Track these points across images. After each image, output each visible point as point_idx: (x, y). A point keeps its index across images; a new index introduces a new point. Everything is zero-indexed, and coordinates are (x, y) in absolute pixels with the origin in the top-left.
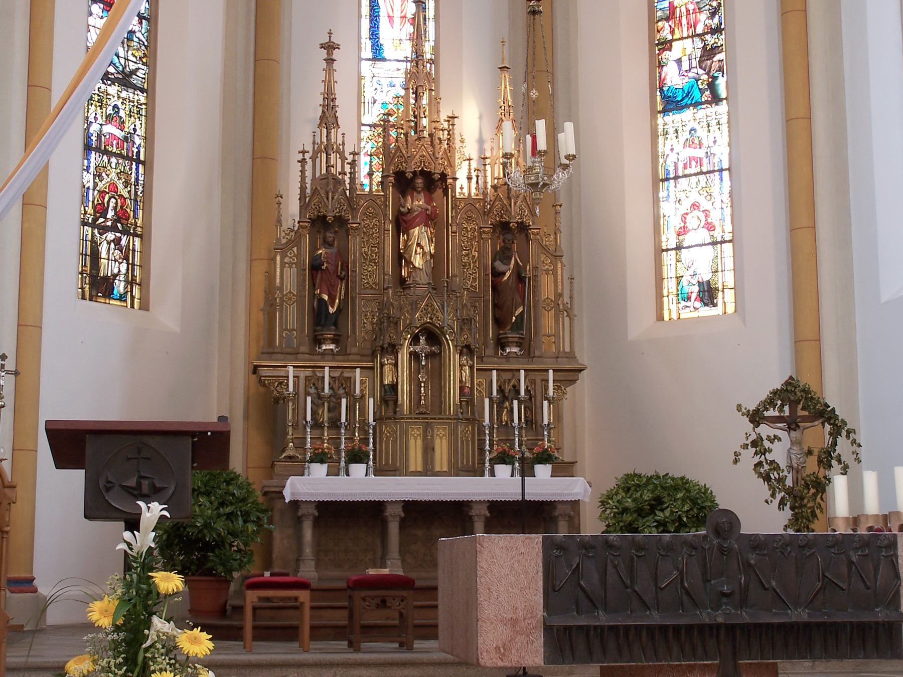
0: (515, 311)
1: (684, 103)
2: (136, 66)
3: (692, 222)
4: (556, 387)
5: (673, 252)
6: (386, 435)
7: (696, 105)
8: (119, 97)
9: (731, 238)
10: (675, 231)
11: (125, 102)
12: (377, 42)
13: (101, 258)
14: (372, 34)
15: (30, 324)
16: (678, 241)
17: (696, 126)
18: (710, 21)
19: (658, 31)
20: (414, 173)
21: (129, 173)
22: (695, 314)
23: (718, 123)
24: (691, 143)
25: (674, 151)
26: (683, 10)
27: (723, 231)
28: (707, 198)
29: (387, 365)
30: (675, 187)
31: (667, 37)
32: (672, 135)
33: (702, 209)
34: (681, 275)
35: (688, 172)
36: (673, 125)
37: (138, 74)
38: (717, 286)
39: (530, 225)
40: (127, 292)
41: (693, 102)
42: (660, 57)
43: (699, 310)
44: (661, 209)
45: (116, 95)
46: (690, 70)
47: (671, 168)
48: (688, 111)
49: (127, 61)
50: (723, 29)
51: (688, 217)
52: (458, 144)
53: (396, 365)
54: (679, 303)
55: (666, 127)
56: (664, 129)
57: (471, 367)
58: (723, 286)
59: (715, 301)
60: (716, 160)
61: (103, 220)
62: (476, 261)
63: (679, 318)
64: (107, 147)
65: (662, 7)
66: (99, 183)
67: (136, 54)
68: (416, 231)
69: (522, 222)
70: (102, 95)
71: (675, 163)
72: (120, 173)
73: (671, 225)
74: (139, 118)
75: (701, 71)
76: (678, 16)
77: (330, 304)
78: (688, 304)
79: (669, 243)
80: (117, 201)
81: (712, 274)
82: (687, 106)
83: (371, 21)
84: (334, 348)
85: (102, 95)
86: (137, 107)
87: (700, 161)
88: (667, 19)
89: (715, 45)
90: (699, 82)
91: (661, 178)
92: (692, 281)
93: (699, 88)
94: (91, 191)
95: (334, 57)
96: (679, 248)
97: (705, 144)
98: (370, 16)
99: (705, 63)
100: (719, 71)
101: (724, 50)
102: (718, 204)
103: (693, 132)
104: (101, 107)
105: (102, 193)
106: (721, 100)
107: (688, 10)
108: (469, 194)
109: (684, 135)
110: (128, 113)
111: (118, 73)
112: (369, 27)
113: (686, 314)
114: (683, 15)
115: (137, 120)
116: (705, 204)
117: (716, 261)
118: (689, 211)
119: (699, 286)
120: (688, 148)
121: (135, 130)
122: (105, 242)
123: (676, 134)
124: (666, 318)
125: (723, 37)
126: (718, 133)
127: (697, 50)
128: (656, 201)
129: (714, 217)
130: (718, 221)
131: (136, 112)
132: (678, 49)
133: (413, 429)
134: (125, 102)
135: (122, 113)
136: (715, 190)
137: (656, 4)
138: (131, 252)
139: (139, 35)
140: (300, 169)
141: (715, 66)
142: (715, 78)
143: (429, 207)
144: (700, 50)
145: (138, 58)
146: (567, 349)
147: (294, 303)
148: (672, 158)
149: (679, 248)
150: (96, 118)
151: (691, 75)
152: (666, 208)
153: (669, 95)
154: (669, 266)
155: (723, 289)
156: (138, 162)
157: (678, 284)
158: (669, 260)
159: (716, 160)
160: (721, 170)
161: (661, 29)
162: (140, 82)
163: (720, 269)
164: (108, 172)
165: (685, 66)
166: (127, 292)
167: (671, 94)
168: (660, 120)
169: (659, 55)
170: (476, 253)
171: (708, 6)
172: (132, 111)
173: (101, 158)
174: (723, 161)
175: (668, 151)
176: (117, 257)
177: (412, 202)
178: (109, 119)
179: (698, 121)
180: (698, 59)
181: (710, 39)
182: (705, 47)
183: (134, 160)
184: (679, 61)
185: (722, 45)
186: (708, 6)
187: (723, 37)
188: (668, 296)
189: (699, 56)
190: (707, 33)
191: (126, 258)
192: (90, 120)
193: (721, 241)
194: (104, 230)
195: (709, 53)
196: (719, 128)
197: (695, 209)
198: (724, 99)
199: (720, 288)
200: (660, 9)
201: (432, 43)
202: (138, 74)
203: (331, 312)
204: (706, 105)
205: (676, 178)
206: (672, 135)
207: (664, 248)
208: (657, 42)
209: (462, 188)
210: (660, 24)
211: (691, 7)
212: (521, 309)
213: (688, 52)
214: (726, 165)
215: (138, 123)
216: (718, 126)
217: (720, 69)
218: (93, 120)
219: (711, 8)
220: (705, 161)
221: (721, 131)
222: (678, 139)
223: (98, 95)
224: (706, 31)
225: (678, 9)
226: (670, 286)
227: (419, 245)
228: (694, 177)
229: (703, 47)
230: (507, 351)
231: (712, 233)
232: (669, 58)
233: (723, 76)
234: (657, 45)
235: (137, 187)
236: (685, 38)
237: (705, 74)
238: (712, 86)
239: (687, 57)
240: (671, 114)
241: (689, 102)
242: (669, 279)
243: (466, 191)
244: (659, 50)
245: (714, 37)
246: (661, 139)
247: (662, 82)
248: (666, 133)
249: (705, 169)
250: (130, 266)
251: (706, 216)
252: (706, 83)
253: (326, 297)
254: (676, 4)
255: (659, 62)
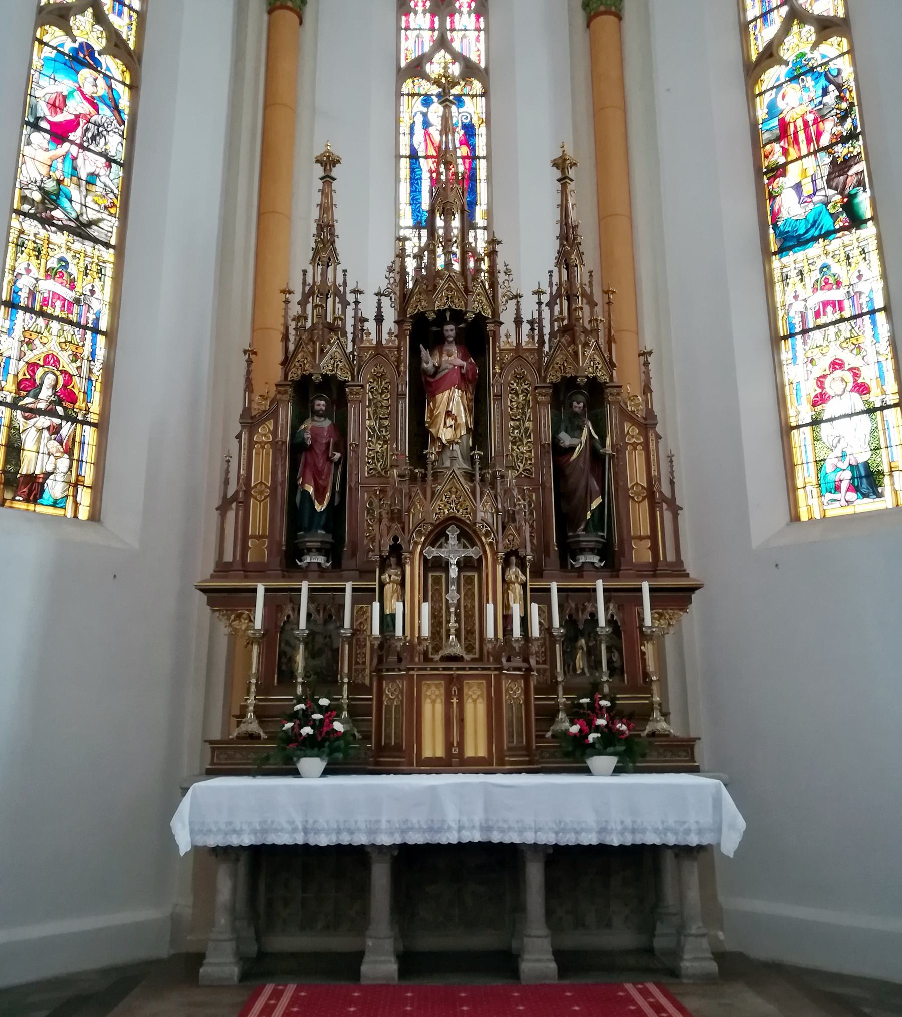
0: (591, 502)
1: (809, 236)
2: (99, 216)
3: (833, 385)
4: (657, 616)
5: (809, 429)
6: (387, 696)
7: (826, 235)
8: (69, 249)
9: (897, 401)
10: (808, 401)
11: (77, 256)
12: (419, 207)
13: (23, 450)
14: (413, 199)
15: (251, 569)
16: (814, 413)
17: (829, 261)
18: (840, 127)
19: (766, 157)
20: (441, 314)
21: (80, 344)
22: (849, 510)
23: (863, 252)
24: (824, 284)
25: (800, 299)
26: (800, 123)
27: (884, 392)
28: (855, 351)
29: (389, 583)
30: (804, 343)
31: (779, 160)
32: (794, 278)
33: (847, 367)
34: (822, 458)
35: (822, 321)
36: (794, 266)
37: (101, 225)
38: (880, 468)
39: (607, 383)
40: (67, 496)
41: (823, 232)
42: (770, 187)
43: (855, 503)
44: (786, 374)
45: (63, 246)
46: (814, 194)
47: (797, 320)
48: (816, 245)
49: (84, 207)
50: (860, 133)
51: (827, 382)
52: (501, 278)
53: (402, 584)
54: (822, 495)
55: (785, 270)
56: (782, 273)
57: (524, 586)
58: (891, 468)
59: (880, 490)
60: (864, 300)
61: (32, 400)
62: (530, 434)
63: (824, 517)
64: (45, 308)
65: (768, 127)
66: (28, 353)
67: (100, 202)
68: (442, 397)
69: (595, 378)
70: (41, 243)
71: (801, 313)
72: (65, 342)
73: (803, 393)
74: (100, 278)
75: (831, 192)
76: (792, 132)
77: (317, 498)
78: (837, 496)
79: (800, 417)
80: (57, 376)
81: (870, 453)
82: (815, 239)
83: (412, 184)
84: (322, 562)
85: (41, 243)
86: (97, 265)
87: (841, 305)
88: (778, 139)
89: (849, 155)
90: (829, 206)
91: (782, 335)
92: (840, 465)
93: (830, 214)
94: (13, 363)
95: (333, 174)
96: (816, 422)
97: (845, 281)
98: (411, 179)
99: (836, 180)
100: (859, 185)
101: (864, 158)
102: (872, 357)
103: (825, 270)
104: (37, 257)
105: (32, 367)
106: (866, 221)
107: (806, 124)
108: (519, 343)
109: (813, 277)
110: (82, 269)
111: (70, 220)
112: (409, 192)
113: (834, 511)
114: (799, 129)
115: (97, 280)
116: (850, 359)
117: (876, 434)
118: (828, 372)
119: (852, 471)
120: (819, 291)
121: (93, 292)
122: (33, 429)
123: (800, 277)
124: (804, 517)
125: (861, 142)
126: (863, 266)
127: (823, 168)
128: (777, 366)
129: (868, 376)
130: (874, 381)
131: (95, 270)
132: (794, 173)
133: (429, 686)
134: (77, 256)
135: (72, 269)
136: (866, 339)
137: (760, 126)
138: (77, 444)
139: (103, 179)
140: (283, 314)
141: (852, 180)
142: (852, 197)
143: (465, 363)
144: (827, 167)
145: (103, 206)
146: (671, 558)
147: (266, 497)
148: (798, 306)
149: (816, 422)
150: (28, 271)
151: (815, 199)
152: (793, 373)
153: (786, 230)
154: (803, 448)
155: (892, 471)
156: (96, 331)
157: (819, 470)
158: (802, 439)
159: (864, 300)
160: (872, 312)
161: (770, 153)
162: (104, 236)
163: (883, 445)
164: (44, 340)
165: (808, 189)
166: (67, 496)
167: (790, 229)
168: (776, 262)
169: (769, 184)
170: (531, 423)
171: (835, 111)
172: (89, 268)
173: (33, 320)
174: (875, 300)
175: (789, 299)
176: (53, 450)
177: (441, 356)
178: (50, 274)
179: (831, 255)
180: (825, 179)
181: (841, 150)
182: (834, 163)
183: (89, 329)
184: (798, 187)
185: (860, 153)
186: (835, 111)
187: (861, 142)
188: (804, 487)
189: (826, 173)
190: (836, 143)
191: (69, 451)
192: (17, 271)
193: (881, 406)
194: (31, 412)
195: (840, 167)
196: (865, 259)
197: (836, 369)
198: (869, 220)
199: (886, 470)
200: (767, 130)
201: (484, 207)
202: (101, 225)
203: (318, 510)
204: (841, 233)
205: (805, 332)
206: (794, 278)
207: (793, 424)
208: (765, 170)
209: (507, 336)
210: (768, 147)
211: (810, 118)
212: (599, 500)
213: (810, 172)
214: (879, 303)
215: (98, 284)
216: (864, 256)
217: (860, 183)
218: (23, 272)
219: (839, 112)
220: (847, 304)
221: (868, 262)
222: (803, 283)
223: (34, 242)
224: (834, 141)
225: (792, 125)
226: (805, 475)
227: (448, 413)
228: (831, 327)
229: (831, 162)
230: (581, 561)
231: (866, 397)
232: (784, 185)
233: (864, 190)
234: (766, 173)
235: (92, 362)
236: (805, 156)
237: (837, 194)
238: (849, 207)
239: (809, 179)
240: (791, 253)
241: (817, 234)
242: (805, 465)
243: (513, 339)
244: (768, 179)
245: (847, 145)
246: (778, 287)
247: (775, 216)
248: (785, 279)
249: (847, 314)
250: (75, 463)
251: (856, 375)
252: (839, 205)
253: (311, 490)
254: (787, 119)
255: (770, 193)
